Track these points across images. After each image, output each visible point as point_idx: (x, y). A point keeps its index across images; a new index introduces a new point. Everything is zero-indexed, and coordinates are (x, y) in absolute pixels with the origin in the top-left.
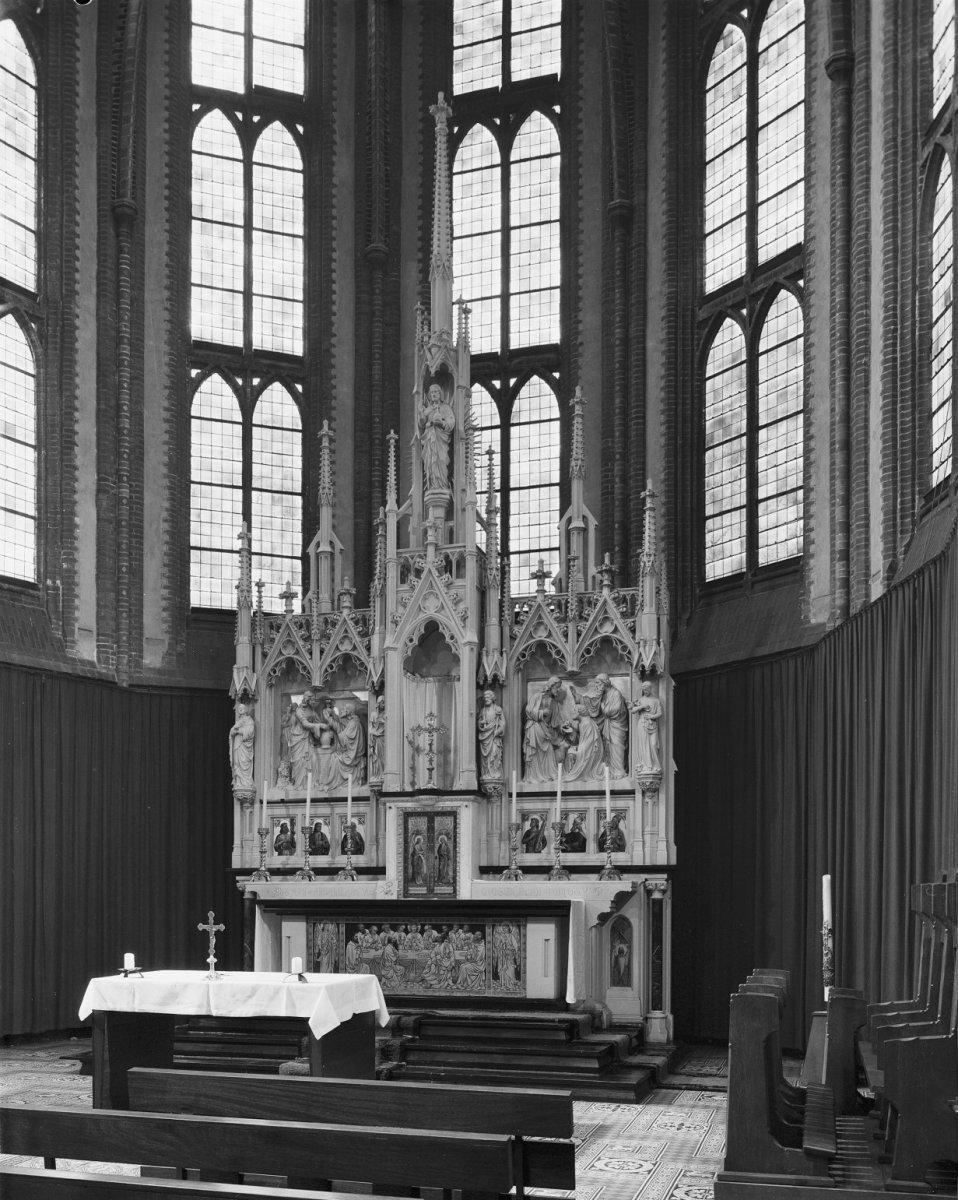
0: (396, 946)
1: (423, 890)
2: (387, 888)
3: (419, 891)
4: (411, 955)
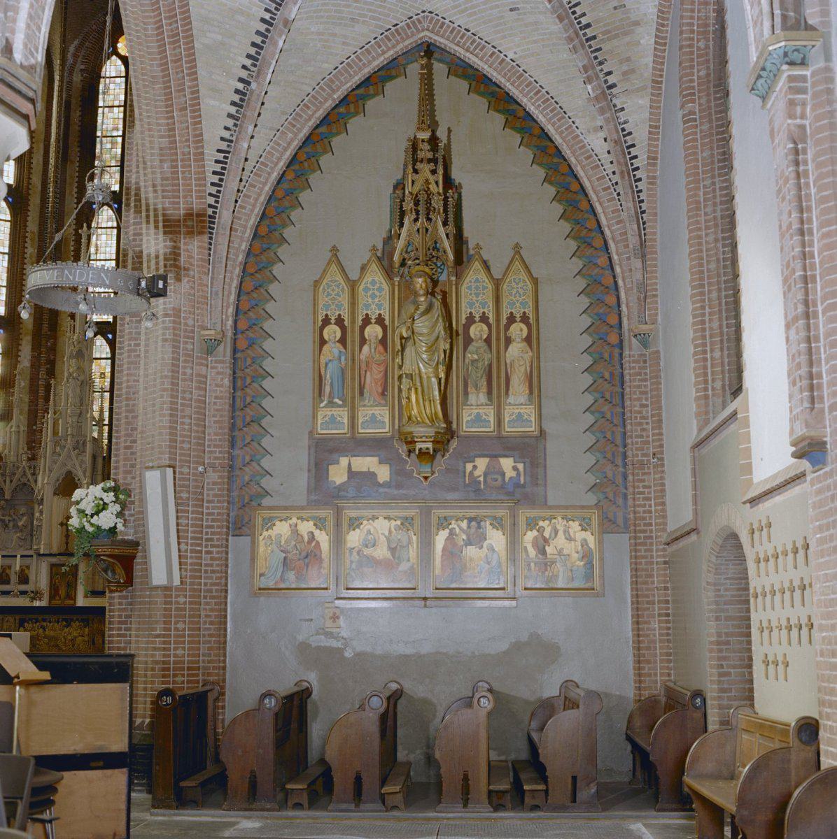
0: (44, 629)
1: (59, 602)
2: (43, 603)
3: (57, 602)
4: (52, 633)
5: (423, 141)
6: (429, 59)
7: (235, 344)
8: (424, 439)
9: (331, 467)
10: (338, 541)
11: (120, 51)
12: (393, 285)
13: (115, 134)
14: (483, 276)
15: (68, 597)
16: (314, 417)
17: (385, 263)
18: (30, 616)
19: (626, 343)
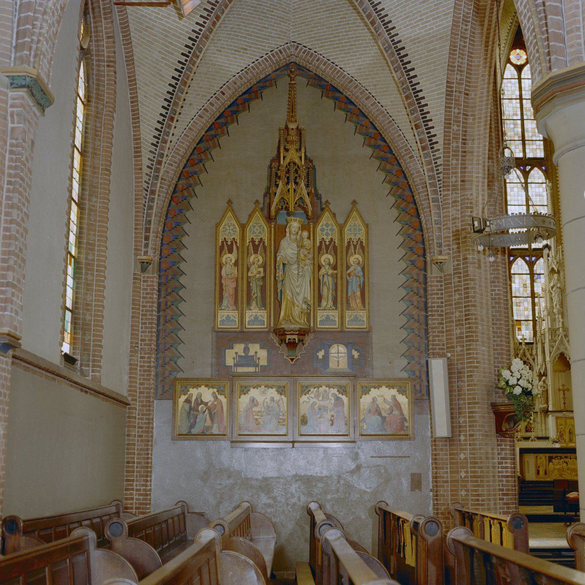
0: (567, 463)
5: (292, 129)
6: (294, 74)
7: (160, 266)
8: (292, 332)
9: (227, 351)
10: (232, 403)
11: (512, 61)
12: (270, 227)
13: (515, 118)
14: (331, 222)
15: (571, 440)
16: (215, 316)
17: (266, 212)
18: (556, 455)
19: (429, 268)
